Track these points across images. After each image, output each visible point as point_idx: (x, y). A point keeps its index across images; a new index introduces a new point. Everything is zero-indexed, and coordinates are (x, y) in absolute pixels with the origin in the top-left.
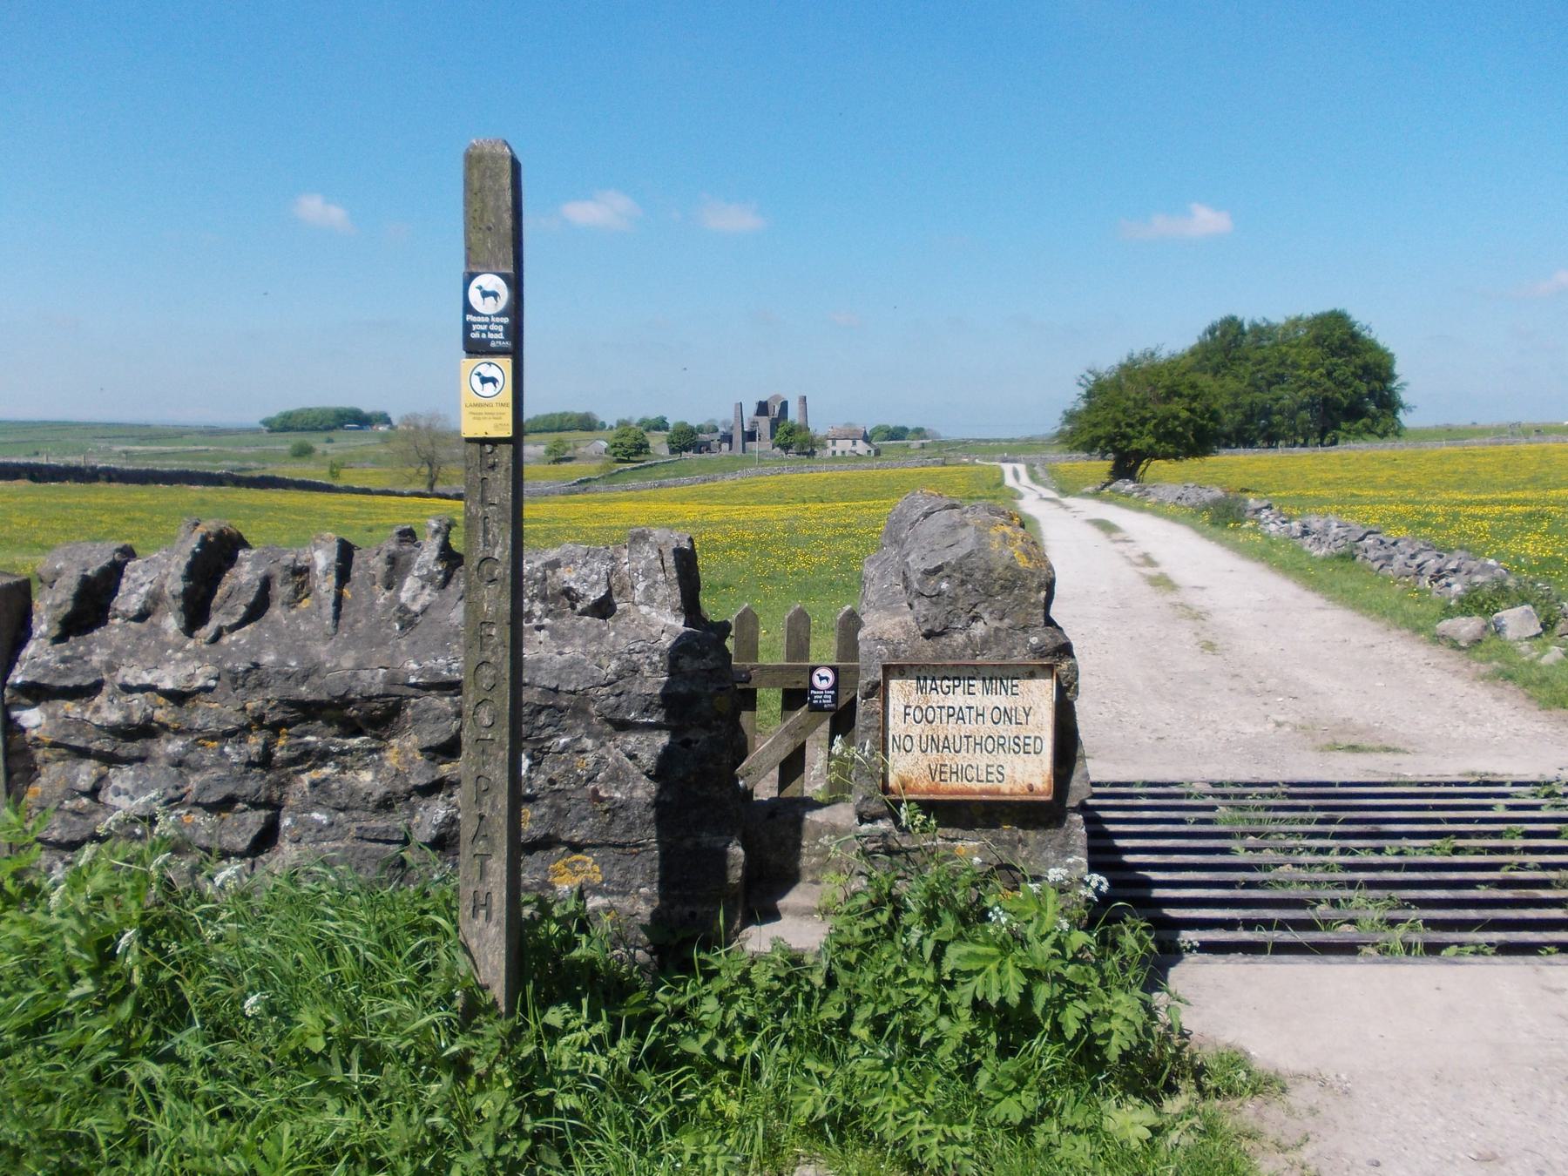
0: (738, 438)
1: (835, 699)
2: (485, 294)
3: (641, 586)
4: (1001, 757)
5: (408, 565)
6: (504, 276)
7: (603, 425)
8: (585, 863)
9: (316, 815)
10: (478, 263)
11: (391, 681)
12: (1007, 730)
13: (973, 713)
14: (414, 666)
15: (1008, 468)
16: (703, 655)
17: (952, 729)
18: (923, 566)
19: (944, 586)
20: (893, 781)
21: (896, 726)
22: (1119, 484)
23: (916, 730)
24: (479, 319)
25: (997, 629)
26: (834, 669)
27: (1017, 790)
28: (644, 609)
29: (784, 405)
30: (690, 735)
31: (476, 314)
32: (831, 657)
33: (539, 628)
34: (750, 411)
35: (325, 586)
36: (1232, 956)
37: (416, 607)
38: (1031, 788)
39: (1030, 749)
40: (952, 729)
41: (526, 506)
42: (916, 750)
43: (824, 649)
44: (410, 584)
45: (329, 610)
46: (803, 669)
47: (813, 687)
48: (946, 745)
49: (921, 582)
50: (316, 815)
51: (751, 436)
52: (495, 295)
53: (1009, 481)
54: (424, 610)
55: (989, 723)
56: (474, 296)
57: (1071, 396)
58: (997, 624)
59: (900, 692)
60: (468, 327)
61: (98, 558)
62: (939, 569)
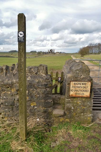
0: (48, 53)
1: (61, 81)
2: (21, 34)
3: (41, 71)
4: (84, 92)
5: (14, 68)
6: (23, 32)
7: (64, 112)
8: (34, 103)
9: (4, 97)
10: (20, 30)
11: (12, 82)
12: (85, 89)
13: (81, 87)
14: (14, 81)
15: (71, 56)
16: (48, 80)
17: (78, 89)
18: (75, 69)
19: (78, 72)
20: (71, 95)
21: (71, 88)
22: (81, 57)
23: (74, 89)
24: (20, 38)
25: (84, 77)
26: (61, 78)
27: (85, 96)
28: (41, 74)
29: (52, 50)
30: (47, 89)
31: (20, 37)
32: (60, 76)
33: (29, 76)
34: (49, 51)
35: (5, 71)
36: (11, 27)
37: (15, 73)
38: (87, 96)
39: (87, 91)
40: (78, 89)
41: (27, 63)
42: (74, 91)
43: (60, 76)
44: (14, 71)
45: (5, 74)
46: (57, 78)
47: (59, 80)
48: (77, 91)
49: (75, 71)
50: (4, 97)
51: (49, 53)
52: (22, 34)
53: (72, 57)
54: (16, 74)
55: (82, 88)
56: (19, 34)
57: (79, 50)
58: (84, 77)
59: (72, 84)
60: (18, 39)
61: (81, 37)
62: (77, 70)
